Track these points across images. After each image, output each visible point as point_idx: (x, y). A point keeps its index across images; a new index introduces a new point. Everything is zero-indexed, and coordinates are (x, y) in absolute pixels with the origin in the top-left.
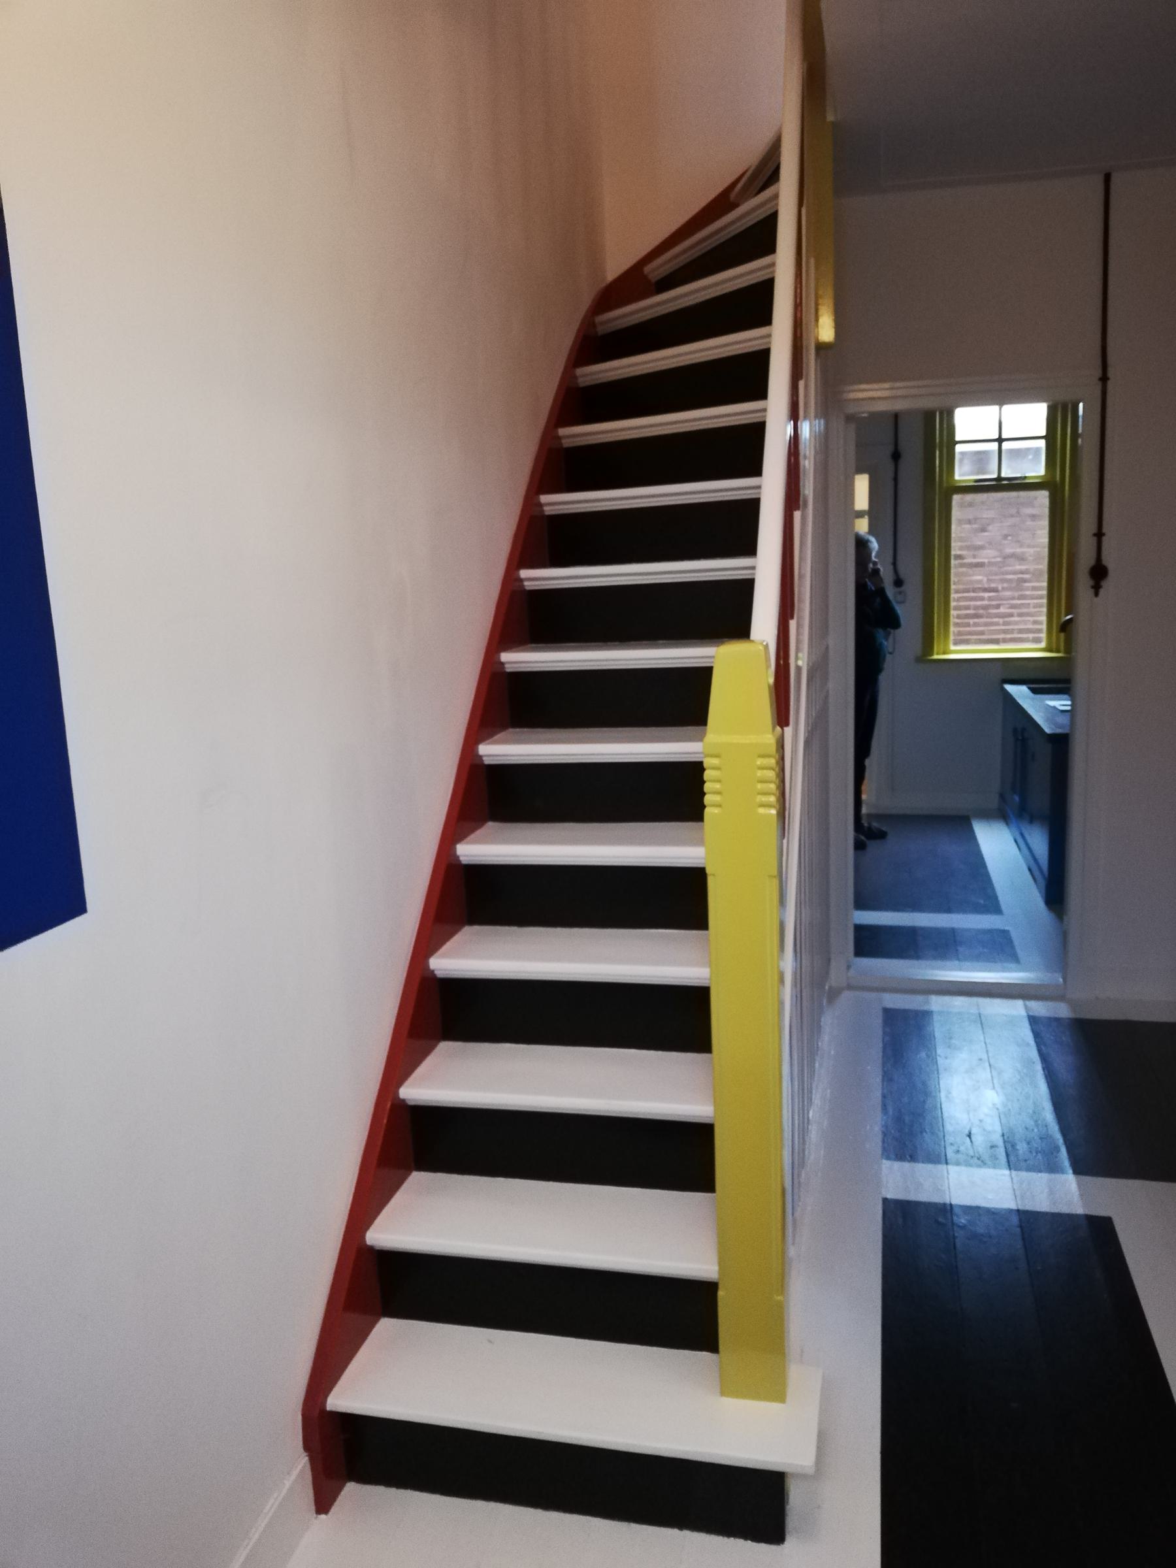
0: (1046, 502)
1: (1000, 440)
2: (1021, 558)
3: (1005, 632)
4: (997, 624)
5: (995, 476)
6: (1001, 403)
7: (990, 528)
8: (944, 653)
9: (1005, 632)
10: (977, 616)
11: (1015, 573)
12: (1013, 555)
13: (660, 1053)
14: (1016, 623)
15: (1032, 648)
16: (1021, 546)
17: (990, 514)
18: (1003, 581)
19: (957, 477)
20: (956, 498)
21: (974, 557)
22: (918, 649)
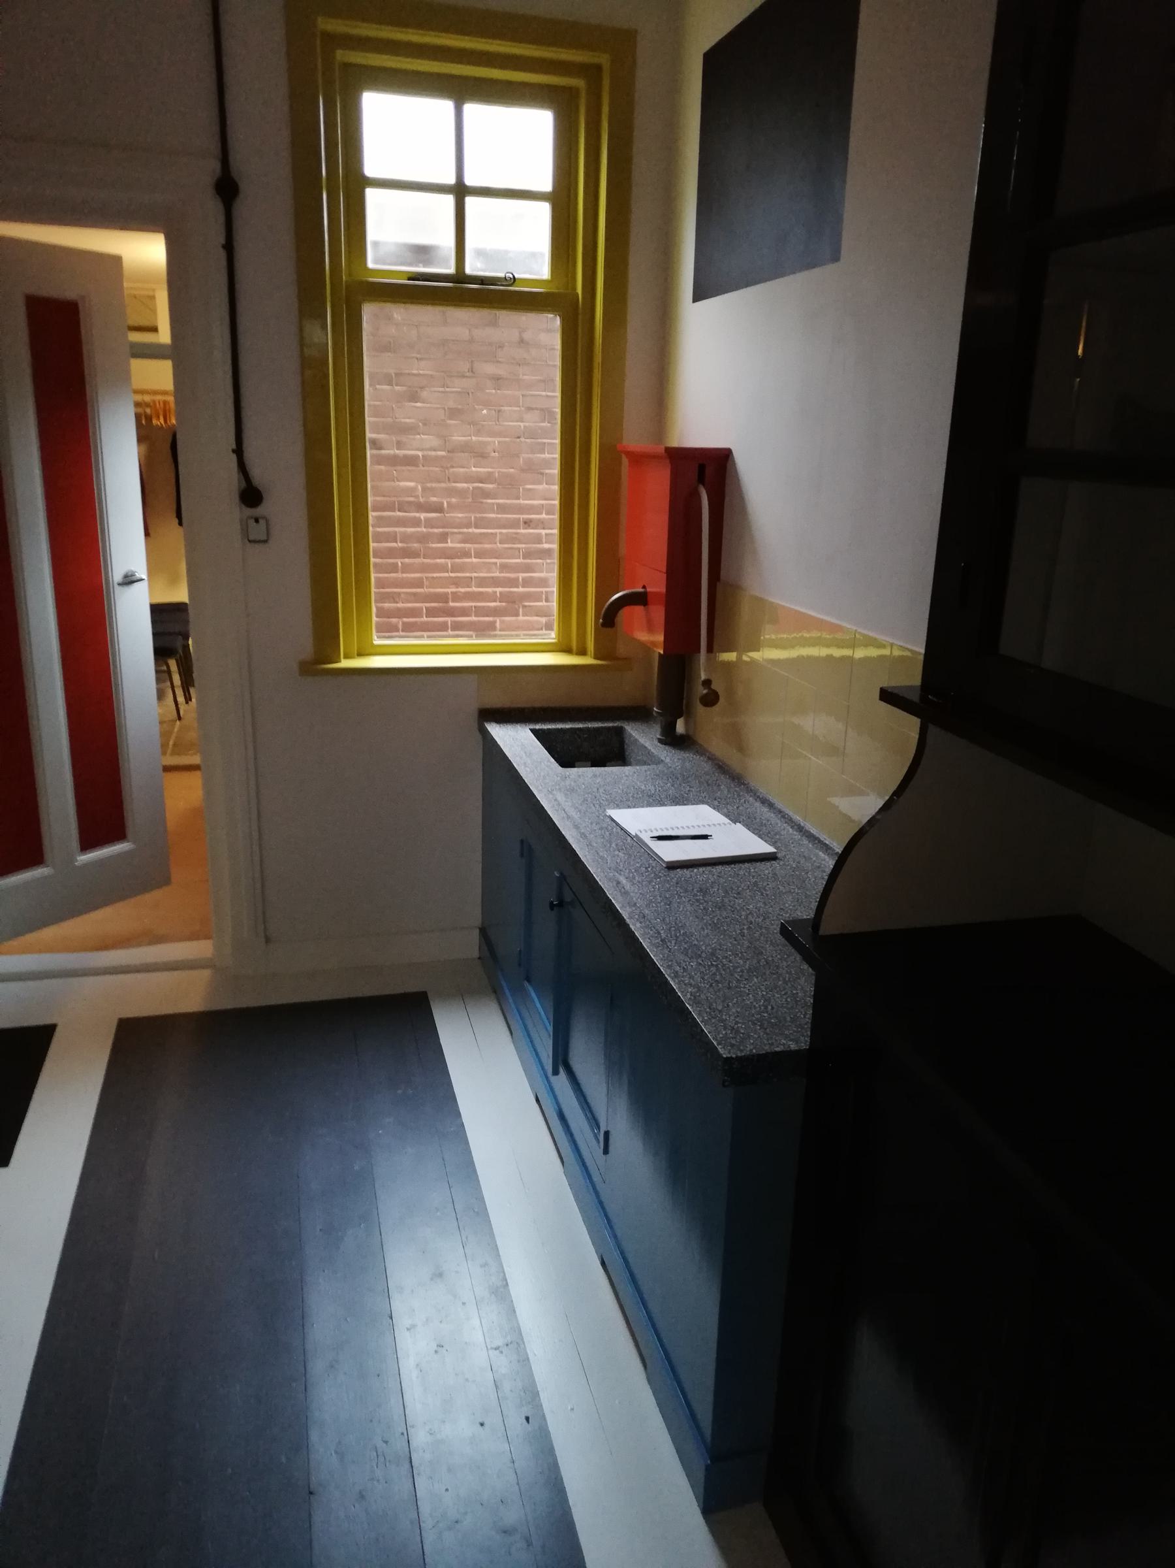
0: (556, 341)
1: (460, 191)
2: (480, 455)
3: (456, 582)
4: (443, 568)
5: (450, 270)
6: (462, 91)
7: (424, 394)
8: (360, 654)
9: (456, 582)
10: (407, 553)
11: (469, 479)
12: (466, 448)
13: (26, 1024)
14: (474, 568)
15: (532, 645)
16: (478, 433)
17: (423, 368)
18: (451, 492)
19: (371, 264)
20: (369, 312)
21: (399, 445)
22: (305, 645)
